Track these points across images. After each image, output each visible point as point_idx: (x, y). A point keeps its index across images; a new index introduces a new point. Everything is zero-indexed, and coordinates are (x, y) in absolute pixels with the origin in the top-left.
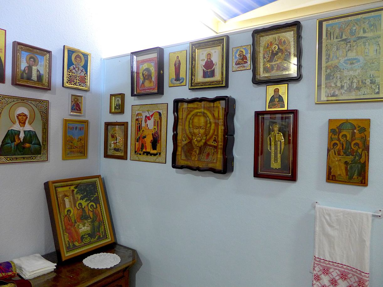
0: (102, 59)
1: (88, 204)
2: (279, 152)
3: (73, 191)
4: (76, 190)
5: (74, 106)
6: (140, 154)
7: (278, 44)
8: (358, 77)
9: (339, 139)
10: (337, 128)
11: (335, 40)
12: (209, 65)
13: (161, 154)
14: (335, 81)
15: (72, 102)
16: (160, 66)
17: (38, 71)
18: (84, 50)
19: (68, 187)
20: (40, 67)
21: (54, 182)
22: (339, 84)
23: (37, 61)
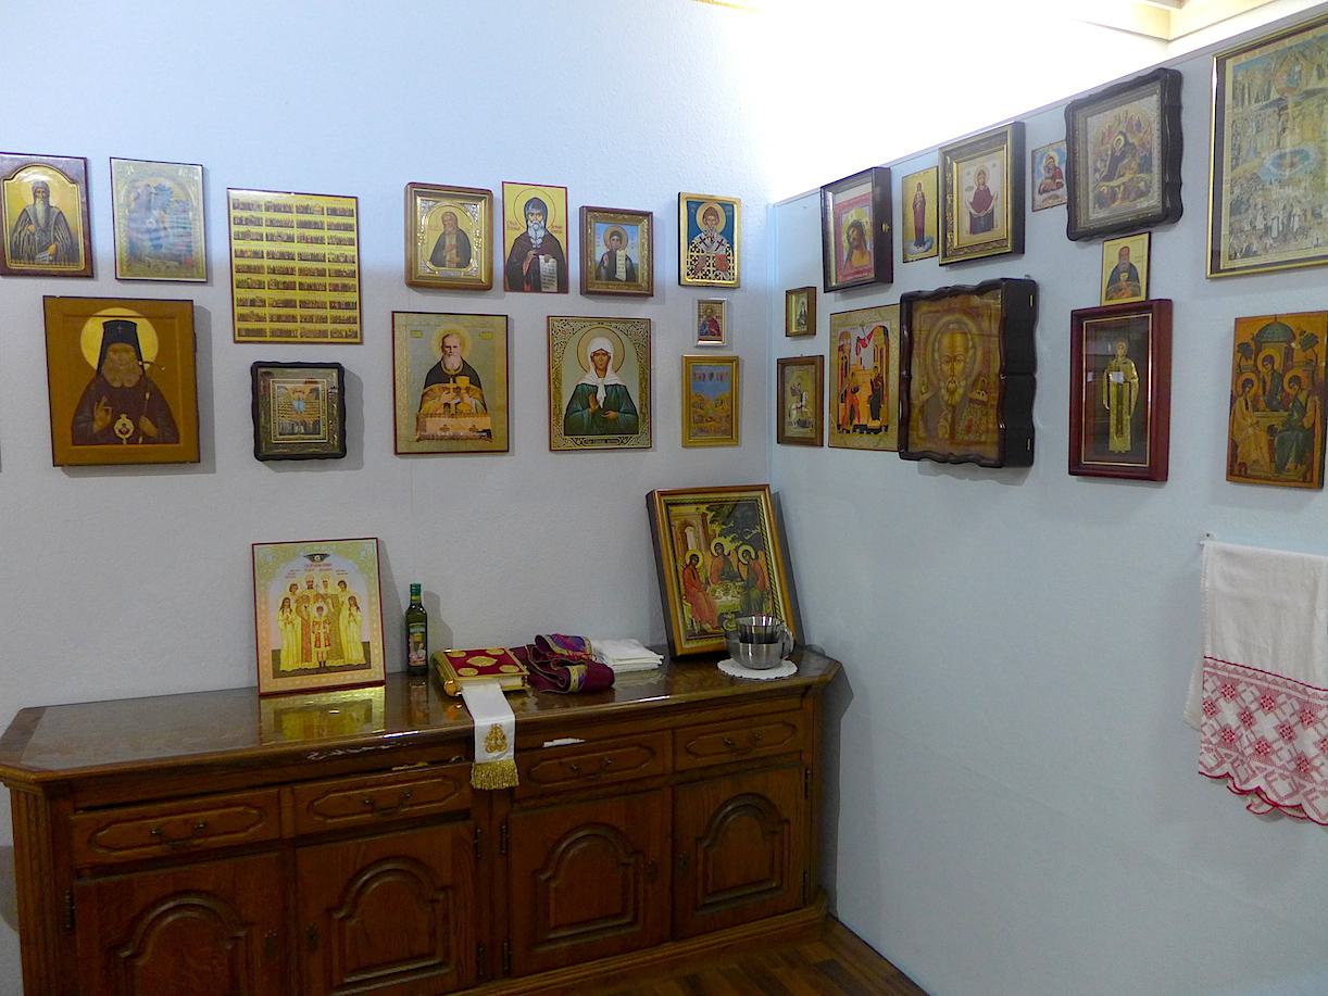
0: (771, 207)
1: (737, 549)
2: (1125, 409)
3: (704, 515)
4: (710, 515)
5: (704, 325)
6: (848, 432)
7: (1124, 131)
8: (1303, 200)
9: (1257, 369)
10: (1253, 339)
11: (1255, 106)
12: (983, 199)
13: (889, 428)
14: (1251, 216)
15: (700, 316)
16: (882, 210)
17: (627, 258)
18: (722, 193)
19: (695, 507)
20: (633, 251)
21: (662, 494)
22: (1260, 225)
23: (624, 237)
